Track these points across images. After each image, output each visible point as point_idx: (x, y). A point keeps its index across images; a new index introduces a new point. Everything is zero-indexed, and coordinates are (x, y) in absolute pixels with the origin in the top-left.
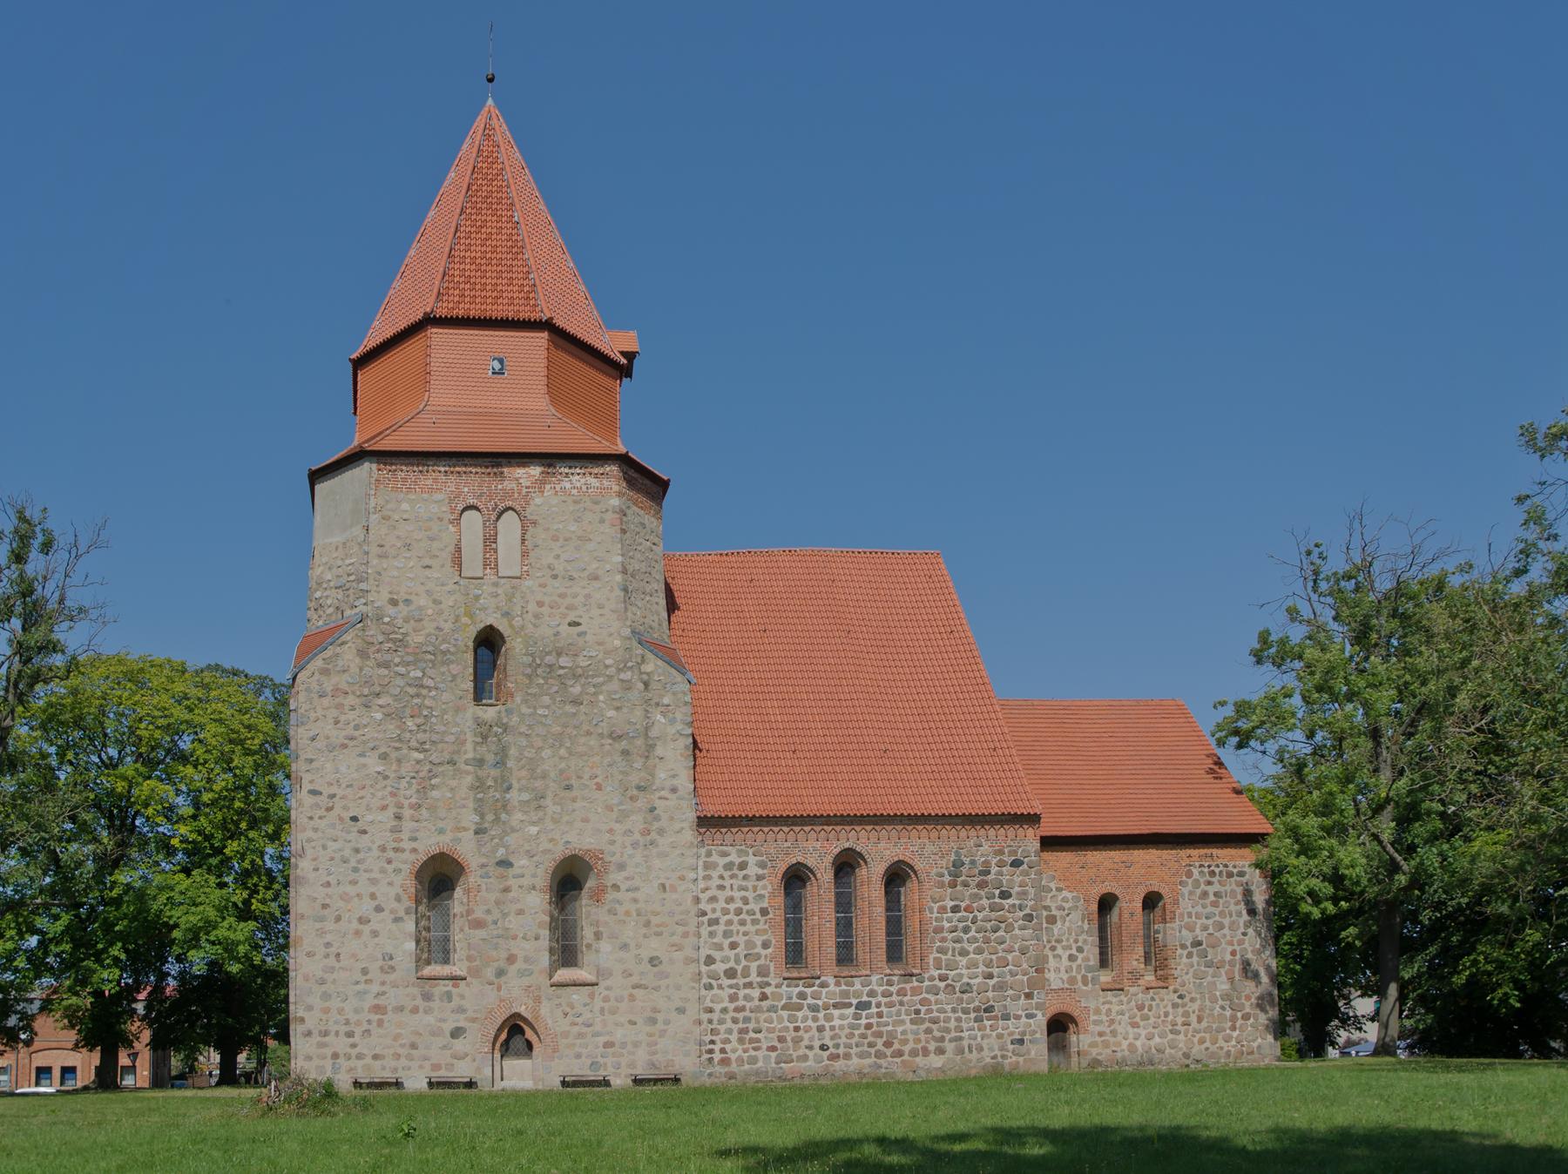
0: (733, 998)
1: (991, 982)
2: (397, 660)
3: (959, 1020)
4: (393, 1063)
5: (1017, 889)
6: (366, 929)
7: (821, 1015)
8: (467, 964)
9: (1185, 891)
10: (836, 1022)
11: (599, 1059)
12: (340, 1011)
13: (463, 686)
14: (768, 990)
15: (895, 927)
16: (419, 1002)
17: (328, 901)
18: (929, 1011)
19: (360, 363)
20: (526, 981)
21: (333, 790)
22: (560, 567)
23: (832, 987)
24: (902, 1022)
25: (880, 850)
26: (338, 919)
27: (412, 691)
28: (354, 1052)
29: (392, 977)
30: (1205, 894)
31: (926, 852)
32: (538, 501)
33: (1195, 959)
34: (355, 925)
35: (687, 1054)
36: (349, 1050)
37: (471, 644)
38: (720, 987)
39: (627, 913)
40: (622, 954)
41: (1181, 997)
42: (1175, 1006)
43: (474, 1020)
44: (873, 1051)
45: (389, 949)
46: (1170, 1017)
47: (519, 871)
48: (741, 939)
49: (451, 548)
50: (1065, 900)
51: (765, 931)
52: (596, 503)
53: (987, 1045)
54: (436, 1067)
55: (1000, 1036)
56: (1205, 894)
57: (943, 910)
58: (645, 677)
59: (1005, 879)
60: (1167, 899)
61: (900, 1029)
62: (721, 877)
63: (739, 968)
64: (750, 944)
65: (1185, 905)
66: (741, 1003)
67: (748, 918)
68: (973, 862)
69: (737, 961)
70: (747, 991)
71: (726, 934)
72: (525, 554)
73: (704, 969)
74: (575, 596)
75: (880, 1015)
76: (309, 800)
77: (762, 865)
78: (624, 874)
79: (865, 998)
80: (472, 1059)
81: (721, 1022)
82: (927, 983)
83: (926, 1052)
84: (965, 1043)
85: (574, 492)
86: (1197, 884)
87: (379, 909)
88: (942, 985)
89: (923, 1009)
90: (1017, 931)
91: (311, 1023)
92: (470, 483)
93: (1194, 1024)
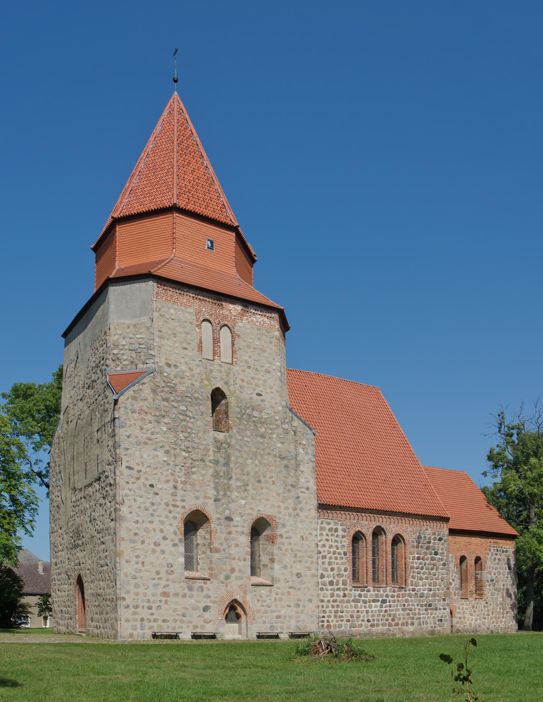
0: (332, 595)
1: (431, 593)
3: (419, 609)
4: (173, 625)
6: (158, 549)
7: (367, 605)
9: (489, 557)
10: (374, 609)
11: (274, 624)
12: (145, 595)
14: (346, 592)
16: (186, 591)
21: (140, 468)
22: (251, 363)
23: (372, 592)
24: (399, 610)
25: (392, 527)
27: (182, 417)
31: (409, 530)
33: (491, 587)
34: (152, 546)
35: (313, 623)
38: (327, 590)
40: (284, 571)
43: (214, 602)
44: (387, 623)
48: (335, 566)
51: (345, 563)
54: (196, 627)
56: (495, 559)
61: (398, 613)
62: (327, 535)
64: (339, 569)
66: (335, 598)
67: (339, 556)
68: (425, 537)
69: (334, 578)
70: (338, 592)
71: (330, 564)
73: (320, 580)
75: (390, 606)
76: (126, 472)
78: (285, 529)
79: (385, 598)
81: (327, 607)
83: (407, 624)
87: (165, 538)
88: (413, 593)
89: (406, 604)
90: (440, 570)
93: (491, 615)
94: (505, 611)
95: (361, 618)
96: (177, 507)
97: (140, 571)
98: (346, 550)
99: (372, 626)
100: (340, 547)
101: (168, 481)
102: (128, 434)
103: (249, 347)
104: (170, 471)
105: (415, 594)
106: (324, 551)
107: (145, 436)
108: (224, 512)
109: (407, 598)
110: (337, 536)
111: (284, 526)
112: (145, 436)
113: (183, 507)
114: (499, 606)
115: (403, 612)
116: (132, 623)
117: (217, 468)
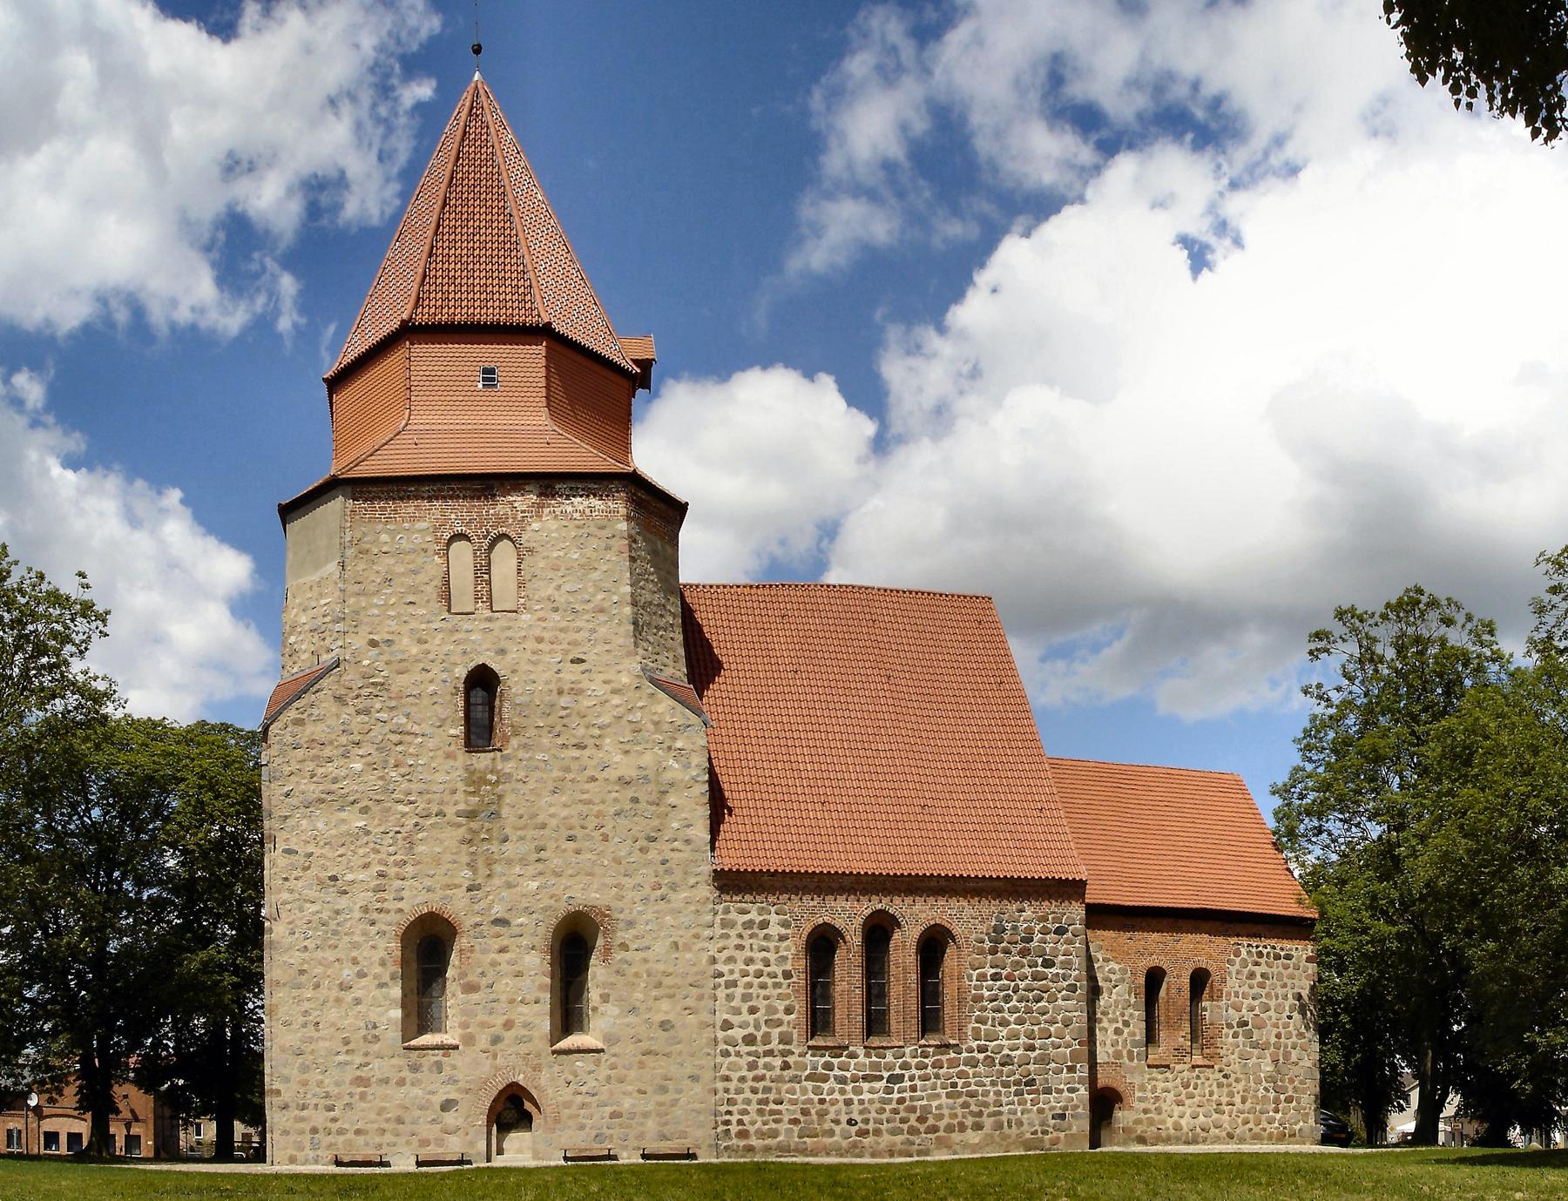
0: (752, 1066)
1: (1033, 1055)
2: (378, 706)
3: (998, 1093)
4: (378, 1140)
5: (1061, 958)
6: (349, 997)
7: (849, 1088)
8: (460, 1031)
9: (1233, 969)
10: (866, 1096)
11: (605, 1130)
12: (320, 1084)
13: (452, 732)
14: (791, 1059)
15: (930, 993)
16: (406, 1073)
17: (305, 967)
18: (967, 1085)
19: (336, 383)
20: (523, 1049)
21: (310, 849)
22: (561, 599)
23: (862, 1059)
24: (938, 1096)
25: (915, 915)
26: (317, 986)
27: (395, 738)
28: (334, 1127)
29: (376, 1047)
30: (1252, 975)
31: (967, 920)
32: (536, 526)
33: (1241, 1039)
34: (335, 993)
35: (701, 1126)
36: (329, 1125)
37: (461, 686)
38: (738, 1054)
39: (637, 975)
40: (631, 1019)
41: (1225, 1076)
42: (1220, 1085)
43: (468, 1091)
44: (905, 1127)
45: (373, 1017)
46: (1215, 1097)
47: (516, 930)
48: (762, 1004)
49: (438, 582)
50: (1112, 971)
51: (788, 996)
52: (602, 528)
53: (1028, 1114)
54: (424, 1143)
55: (1041, 1111)
56: (1252, 975)
57: (982, 978)
58: (656, 718)
59: (1048, 948)
60: (1215, 977)
61: (935, 1104)
62: (740, 936)
63: (759, 1035)
64: (771, 1010)
65: (1232, 984)
66: (760, 1072)
67: (770, 981)
68: (1015, 928)
69: (757, 1027)
70: (767, 1059)
71: (746, 998)
72: (521, 585)
73: (721, 1035)
74: (579, 630)
75: (913, 1089)
76: (283, 861)
77: (785, 925)
78: (633, 932)
79: (898, 1071)
80: (465, 1136)
81: (739, 1091)
82: (965, 1054)
83: (962, 1128)
84: (1004, 1118)
85: (577, 515)
86: (1244, 964)
87: (361, 975)
88: (981, 1056)
89: (960, 1082)
90: (1060, 1002)
91: (286, 1096)
92: (457, 513)
93: (1239, 1105)
94: (1282, 1097)
95: (831, 1116)
96: (388, 912)
97: (311, 1040)
98: (788, 967)
99: (863, 1133)
100: (772, 961)
101: (366, 866)
102: (286, 789)
103: (556, 569)
104: (372, 845)
105: (987, 1057)
106: (732, 972)
107: (321, 787)
108: (490, 907)
109: (962, 1067)
110: (767, 937)
111: (631, 924)
112: (321, 787)
113: (400, 910)
114: (1264, 1084)
115: (951, 1101)
116: (292, 1138)
117: (472, 825)
